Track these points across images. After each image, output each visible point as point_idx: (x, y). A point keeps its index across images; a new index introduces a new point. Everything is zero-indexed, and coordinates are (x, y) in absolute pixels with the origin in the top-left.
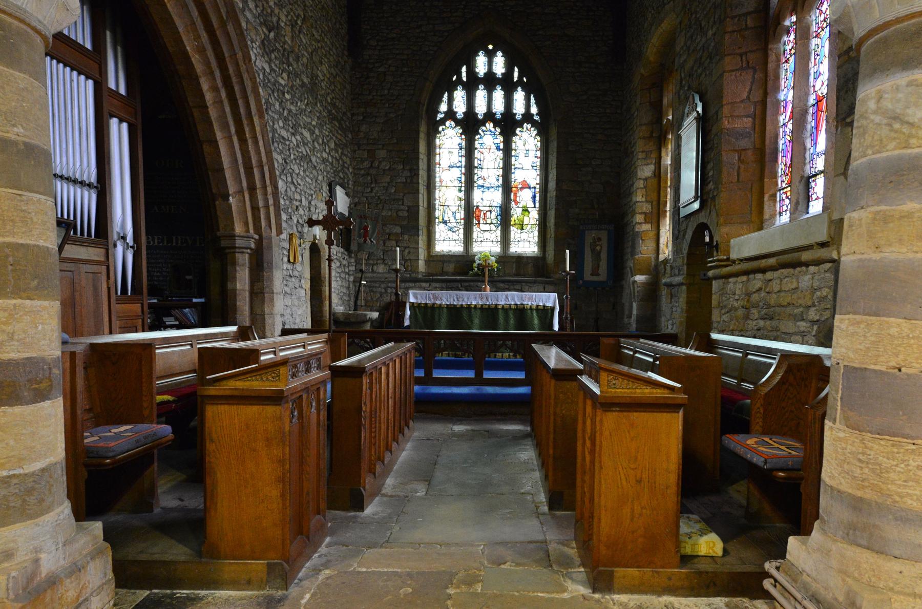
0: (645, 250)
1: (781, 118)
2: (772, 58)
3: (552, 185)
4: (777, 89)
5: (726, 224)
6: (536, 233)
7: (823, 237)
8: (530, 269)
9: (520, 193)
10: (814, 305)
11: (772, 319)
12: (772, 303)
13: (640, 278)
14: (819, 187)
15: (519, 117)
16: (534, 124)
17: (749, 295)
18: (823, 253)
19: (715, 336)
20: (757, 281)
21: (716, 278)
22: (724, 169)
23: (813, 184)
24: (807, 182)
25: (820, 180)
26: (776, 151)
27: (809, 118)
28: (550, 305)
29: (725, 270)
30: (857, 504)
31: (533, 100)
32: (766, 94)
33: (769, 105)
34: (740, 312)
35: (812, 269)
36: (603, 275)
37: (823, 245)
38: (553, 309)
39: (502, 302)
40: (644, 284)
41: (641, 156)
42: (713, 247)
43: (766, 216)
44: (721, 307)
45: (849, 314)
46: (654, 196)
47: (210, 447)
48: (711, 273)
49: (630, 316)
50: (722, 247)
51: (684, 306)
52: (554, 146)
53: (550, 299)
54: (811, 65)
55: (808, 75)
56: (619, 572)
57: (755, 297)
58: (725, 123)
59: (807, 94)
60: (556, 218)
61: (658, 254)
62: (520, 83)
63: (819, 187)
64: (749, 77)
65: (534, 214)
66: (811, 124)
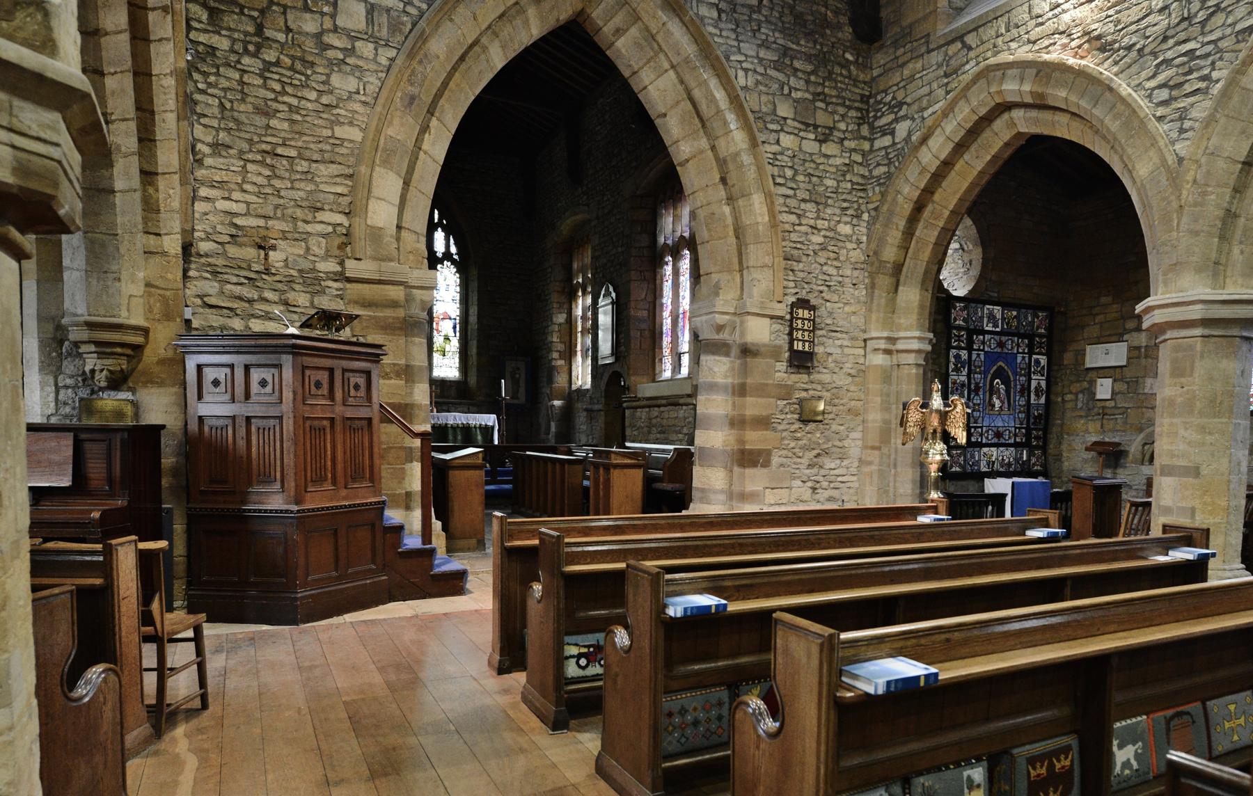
0: (560, 381)
3: (473, 319)
4: (661, 296)
5: (635, 374)
6: (457, 360)
7: (689, 392)
8: (453, 392)
9: (441, 323)
13: (557, 403)
14: (685, 360)
15: (439, 255)
16: (453, 262)
18: (689, 400)
19: (628, 444)
20: (655, 412)
24: (679, 355)
25: (687, 356)
26: (661, 333)
29: (635, 404)
30: (703, 490)
31: (452, 241)
32: (655, 298)
34: (646, 429)
36: (522, 398)
37: (689, 396)
38: (493, 428)
39: (451, 422)
42: (626, 389)
44: (632, 426)
45: (1024, 745)
46: (567, 338)
47: (451, 490)
50: (632, 389)
52: (474, 285)
53: (490, 419)
57: (654, 421)
60: (478, 347)
62: (440, 224)
63: (685, 360)
65: (455, 343)
66: (681, 324)
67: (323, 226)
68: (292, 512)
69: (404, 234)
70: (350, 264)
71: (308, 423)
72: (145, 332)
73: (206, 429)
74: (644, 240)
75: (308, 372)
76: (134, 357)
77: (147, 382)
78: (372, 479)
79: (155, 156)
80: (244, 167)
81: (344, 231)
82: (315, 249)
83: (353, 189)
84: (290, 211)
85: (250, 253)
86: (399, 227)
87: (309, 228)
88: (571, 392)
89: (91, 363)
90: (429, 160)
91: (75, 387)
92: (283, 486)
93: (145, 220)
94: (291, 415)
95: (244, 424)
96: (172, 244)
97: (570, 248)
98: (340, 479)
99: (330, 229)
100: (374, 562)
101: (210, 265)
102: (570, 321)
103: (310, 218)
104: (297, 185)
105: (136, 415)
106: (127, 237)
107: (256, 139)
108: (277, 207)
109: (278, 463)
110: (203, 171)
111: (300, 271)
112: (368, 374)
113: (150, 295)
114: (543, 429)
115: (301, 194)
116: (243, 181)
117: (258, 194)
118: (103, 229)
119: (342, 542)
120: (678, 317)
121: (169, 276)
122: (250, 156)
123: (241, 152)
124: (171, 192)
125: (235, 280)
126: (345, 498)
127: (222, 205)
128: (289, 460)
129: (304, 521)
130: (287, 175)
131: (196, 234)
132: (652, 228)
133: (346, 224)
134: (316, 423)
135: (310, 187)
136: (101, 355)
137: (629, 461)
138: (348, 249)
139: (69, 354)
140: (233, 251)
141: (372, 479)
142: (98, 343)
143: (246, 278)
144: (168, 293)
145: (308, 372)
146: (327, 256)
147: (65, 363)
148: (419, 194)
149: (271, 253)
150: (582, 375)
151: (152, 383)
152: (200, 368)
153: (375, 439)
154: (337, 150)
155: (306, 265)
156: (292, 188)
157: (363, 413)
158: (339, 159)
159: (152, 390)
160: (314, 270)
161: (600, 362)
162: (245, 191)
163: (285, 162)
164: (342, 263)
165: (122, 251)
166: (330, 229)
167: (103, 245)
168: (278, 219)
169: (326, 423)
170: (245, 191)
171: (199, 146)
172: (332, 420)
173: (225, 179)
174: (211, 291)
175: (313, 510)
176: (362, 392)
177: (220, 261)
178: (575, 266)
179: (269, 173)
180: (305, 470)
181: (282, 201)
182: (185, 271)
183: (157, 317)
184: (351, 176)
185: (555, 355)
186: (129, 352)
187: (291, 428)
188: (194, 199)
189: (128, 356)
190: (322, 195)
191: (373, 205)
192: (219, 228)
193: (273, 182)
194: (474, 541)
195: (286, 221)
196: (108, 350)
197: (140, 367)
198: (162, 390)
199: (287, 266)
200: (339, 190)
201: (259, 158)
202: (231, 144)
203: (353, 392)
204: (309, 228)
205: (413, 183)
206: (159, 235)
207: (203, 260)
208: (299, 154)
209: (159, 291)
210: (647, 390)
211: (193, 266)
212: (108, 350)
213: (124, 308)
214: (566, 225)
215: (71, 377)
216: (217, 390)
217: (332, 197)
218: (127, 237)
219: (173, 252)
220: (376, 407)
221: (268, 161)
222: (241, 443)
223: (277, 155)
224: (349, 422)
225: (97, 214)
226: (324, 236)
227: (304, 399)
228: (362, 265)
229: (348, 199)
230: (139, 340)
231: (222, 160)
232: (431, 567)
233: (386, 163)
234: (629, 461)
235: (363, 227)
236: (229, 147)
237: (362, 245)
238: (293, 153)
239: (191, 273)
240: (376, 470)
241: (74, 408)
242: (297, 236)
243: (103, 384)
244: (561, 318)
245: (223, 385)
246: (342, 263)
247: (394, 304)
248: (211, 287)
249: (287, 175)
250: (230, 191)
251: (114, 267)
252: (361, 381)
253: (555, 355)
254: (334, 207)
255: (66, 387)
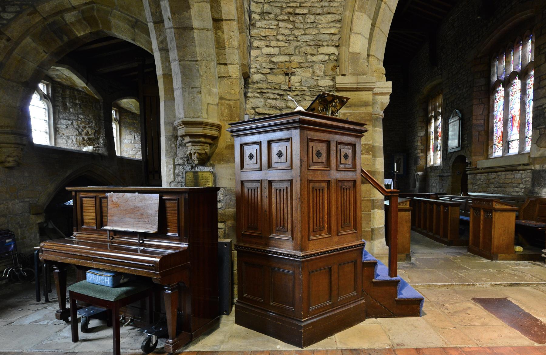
0: (421, 163)
1: (495, 121)
2: (491, 101)
10: (522, 183)
11: (501, 187)
12: (501, 182)
17: (489, 180)
19: (469, 193)
21: (470, 174)
22: (474, 138)
23: (510, 144)
27: (509, 122)
28: (390, 183)
29: (476, 171)
32: (489, 113)
33: (490, 116)
34: (484, 186)
35: (521, 172)
36: (402, 172)
38: (391, 185)
40: (421, 175)
41: (419, 128)
43: (489, 153)
46: (425, 143)
48: (468, 172)
49: (415, 187)
50: (473, 163)
51: (451, 184)
54: (510, 105)
55: (509, 108)
56: (500, 255)
58: (474, 122)
59: (508, 114)
61: (427, 164)
64: (483, 107)
67: (322, 56)
68: (298, 257)
69: (371, 59)
70: (339, 79)
71: (311, 185)
72: (219, 127)
73: (246, 190)
74: (482, 81)
75: (311, 144)
76: (213, 145)
77: (220, 160)
78: (355, 228)
79: (220, 6)
80: (277, 25)
81: (335, 58)
82: (318, 72)
83: (341, 29)
84: (303, 49)
85: (281, 78)
86: (368, 55)
87: (314, 59)
88: (427, 168)
89: (190, 148)
90: (387, 8)
91: (183, 165)
92: (292, 236)
93: (218, 55)
94: (299, 179)
95: (267, 186)
96: (234, 71)
97: (432, 96)
98: (334, 227)
99: (327, 58)
100: (356, 290)
101: (259, 88)
102: (427, 135)
103: (315, 52)
104: (308, 31)
105: (214, 181)
106: (204, 63)
107: (284, 5)
108: (296, 47)
109: (289, 216)
110: (256, 31)
111: (309, 87)
112: (354, 146)
113: (222, 104)
114: (411, 186)
115: (310, 37)
116: (278, 34)
117: (286, 41)
118: (189, 58)
119: (334, 277)
120: (508, 120)
121: (233, 91)
122: (281, 17)
123: (276, 15)
124: (232, 34)
125: (272, 96)
126: (337, 243)
127: (266, 50)
128: (297, 215)
129: (309, 264)
130: (302, 26)
131: (252, 70)
132: (488, 74)
133: (337, 53)
134: (317, 185)
135: (315, 32)
136: (194, 143)
137: (505, 207)
138: (338, 70)
139: (181, 145)
140: (271, 78)
141: (355, 228)
142: (191, 136)
143: (279, 94)
144: (231, 103)
145: (311, 144)
146: (325, 75)
147: (179, 150)
148: (381, 33)
149: (292, 77)
150: (435, 158)
151: (223, 160)
152: (242, 146)
153: (358, 196)
154: (331, 5)
155: (312, 83)
156: (305, 34)
157: (350, 176)
158: (333, 10)
159: (223, 165)
160: (317, 86)
161: (449, 151)
162: (278, 40)
163: (300, 18)
164: (333, 80)
165: (202, 73)
166: (327, 58)
167: (190, 70)
168: (296, 55)
169: (324, 185)
170: (278, 40)
171: (254, 15)
172: (329, 182)
173: (268, 34)
174: (260, 104)
175: (314, 255)
176: (350, 161)
177: (264, 86)
178: (430, 108)
179: (291, 26)
180: (309, 224)
181: (298, 44)
182: (245, 94)
183: (225, 119)
184: (339, 21)
185: (419, 151)
186: (209, 141)
187: (299, 190)
188: (250, 48)
189: (210, 144)
190: (322, 36)
191: (353, 38)
192: (264, 65)
193: (293, 32)
194: (404, 255)
195: (300, 56)
196: (197, 140)
197: (217, 151)
198: (228, 165)
199: (301, 85)
200: (333, 31)
201: (286, 18)
202: (270, 11)
203: (343, 161)
204: (314, 59)
205: (377, 25)
206: (226, 64)
207: (255, 86)
208: (309, 11)
209: (227, 102)
210: (483, 163)
211: (250, 90)
212: (197, 140)
213: (204, 112)
214: (426, 89)
215: (181, 158)
216: (252, 162)
217: (328, 36)
218: (204, 63)
219: (234, 76)
220: (359, 172)
221: (291, 19)
222: (266, 201)
223: (296, 14)
224: (340, 184)
225: (185, 47)
226: (323, 62)
227: (308, 165)
228: (346, 79)
229: (338, 37)
230: (214, 133)
231: (265, 22)
232: (396, 294)
233: (362, 8)
234: (505, 207)
235: (347, 53)
236: (269, 13)
237: (347, 66)
238: (305, 11)
239: (249, 95)
240: (358, 220)
241: (182, 178)
242: (307, 64)
243: (196, 162)
244: (422, 134)
245: (255, 158)
246: (333, 80)
247: (366, 104)
248: (259, 102)
249: (302, 26)
250: (270, 41)
251: (197, 84)
252: (349, 151)
253: (419, 151)
254: (329, 43)
255: (179, 165)
